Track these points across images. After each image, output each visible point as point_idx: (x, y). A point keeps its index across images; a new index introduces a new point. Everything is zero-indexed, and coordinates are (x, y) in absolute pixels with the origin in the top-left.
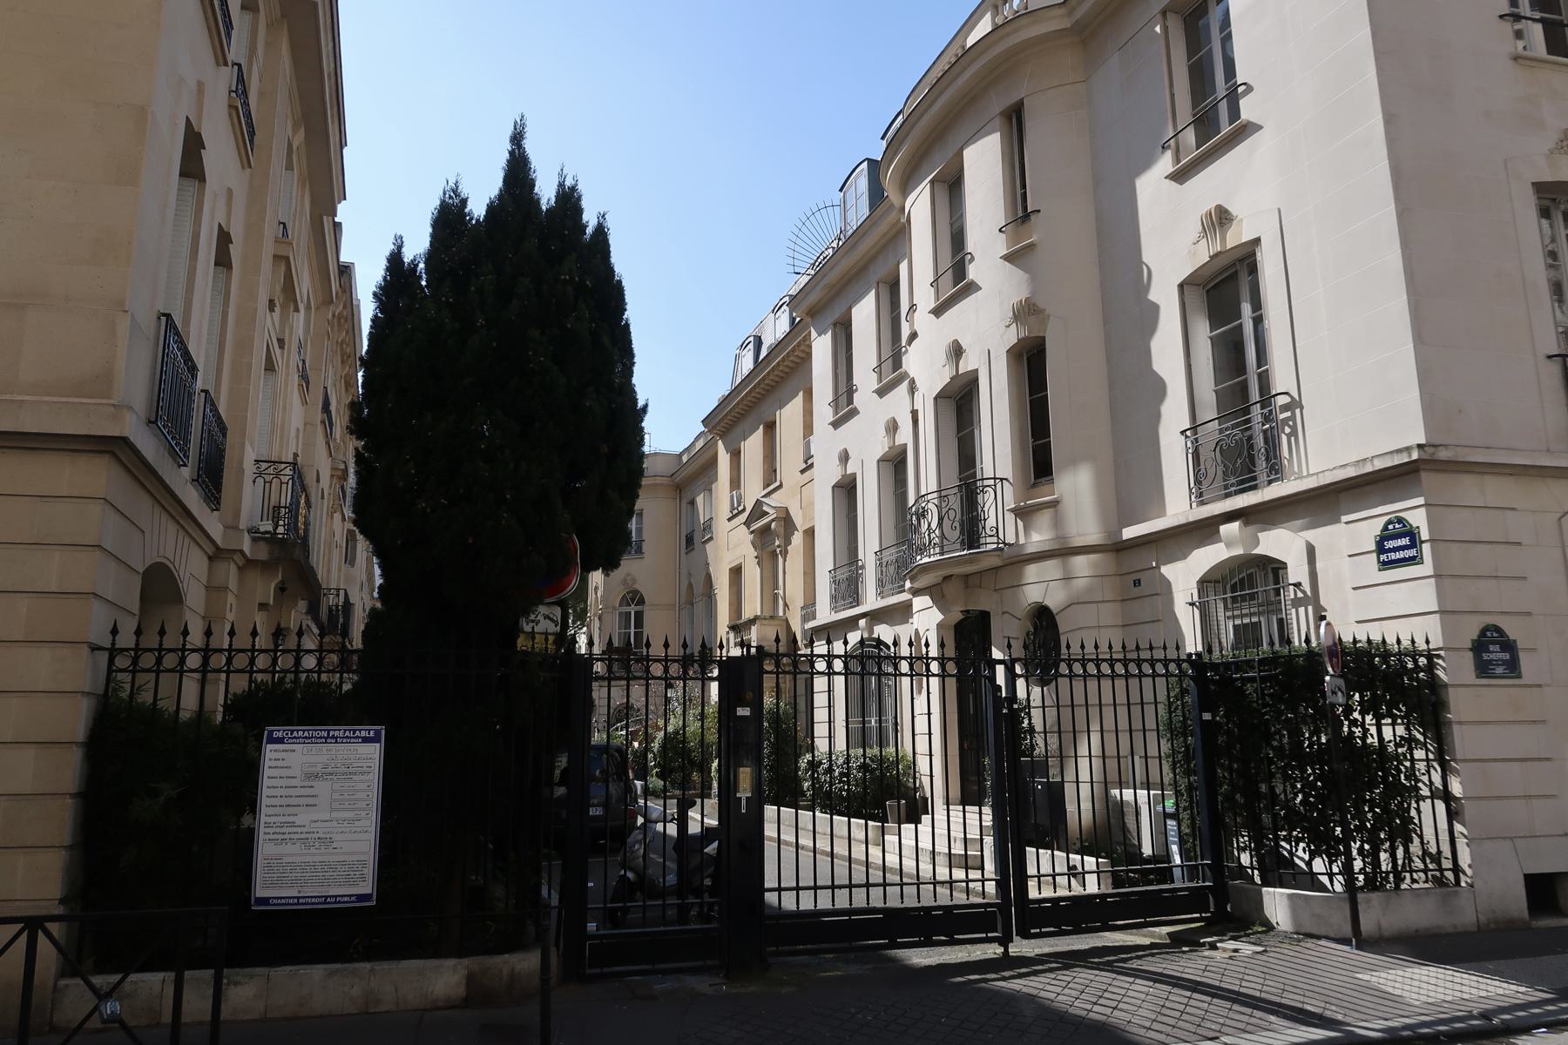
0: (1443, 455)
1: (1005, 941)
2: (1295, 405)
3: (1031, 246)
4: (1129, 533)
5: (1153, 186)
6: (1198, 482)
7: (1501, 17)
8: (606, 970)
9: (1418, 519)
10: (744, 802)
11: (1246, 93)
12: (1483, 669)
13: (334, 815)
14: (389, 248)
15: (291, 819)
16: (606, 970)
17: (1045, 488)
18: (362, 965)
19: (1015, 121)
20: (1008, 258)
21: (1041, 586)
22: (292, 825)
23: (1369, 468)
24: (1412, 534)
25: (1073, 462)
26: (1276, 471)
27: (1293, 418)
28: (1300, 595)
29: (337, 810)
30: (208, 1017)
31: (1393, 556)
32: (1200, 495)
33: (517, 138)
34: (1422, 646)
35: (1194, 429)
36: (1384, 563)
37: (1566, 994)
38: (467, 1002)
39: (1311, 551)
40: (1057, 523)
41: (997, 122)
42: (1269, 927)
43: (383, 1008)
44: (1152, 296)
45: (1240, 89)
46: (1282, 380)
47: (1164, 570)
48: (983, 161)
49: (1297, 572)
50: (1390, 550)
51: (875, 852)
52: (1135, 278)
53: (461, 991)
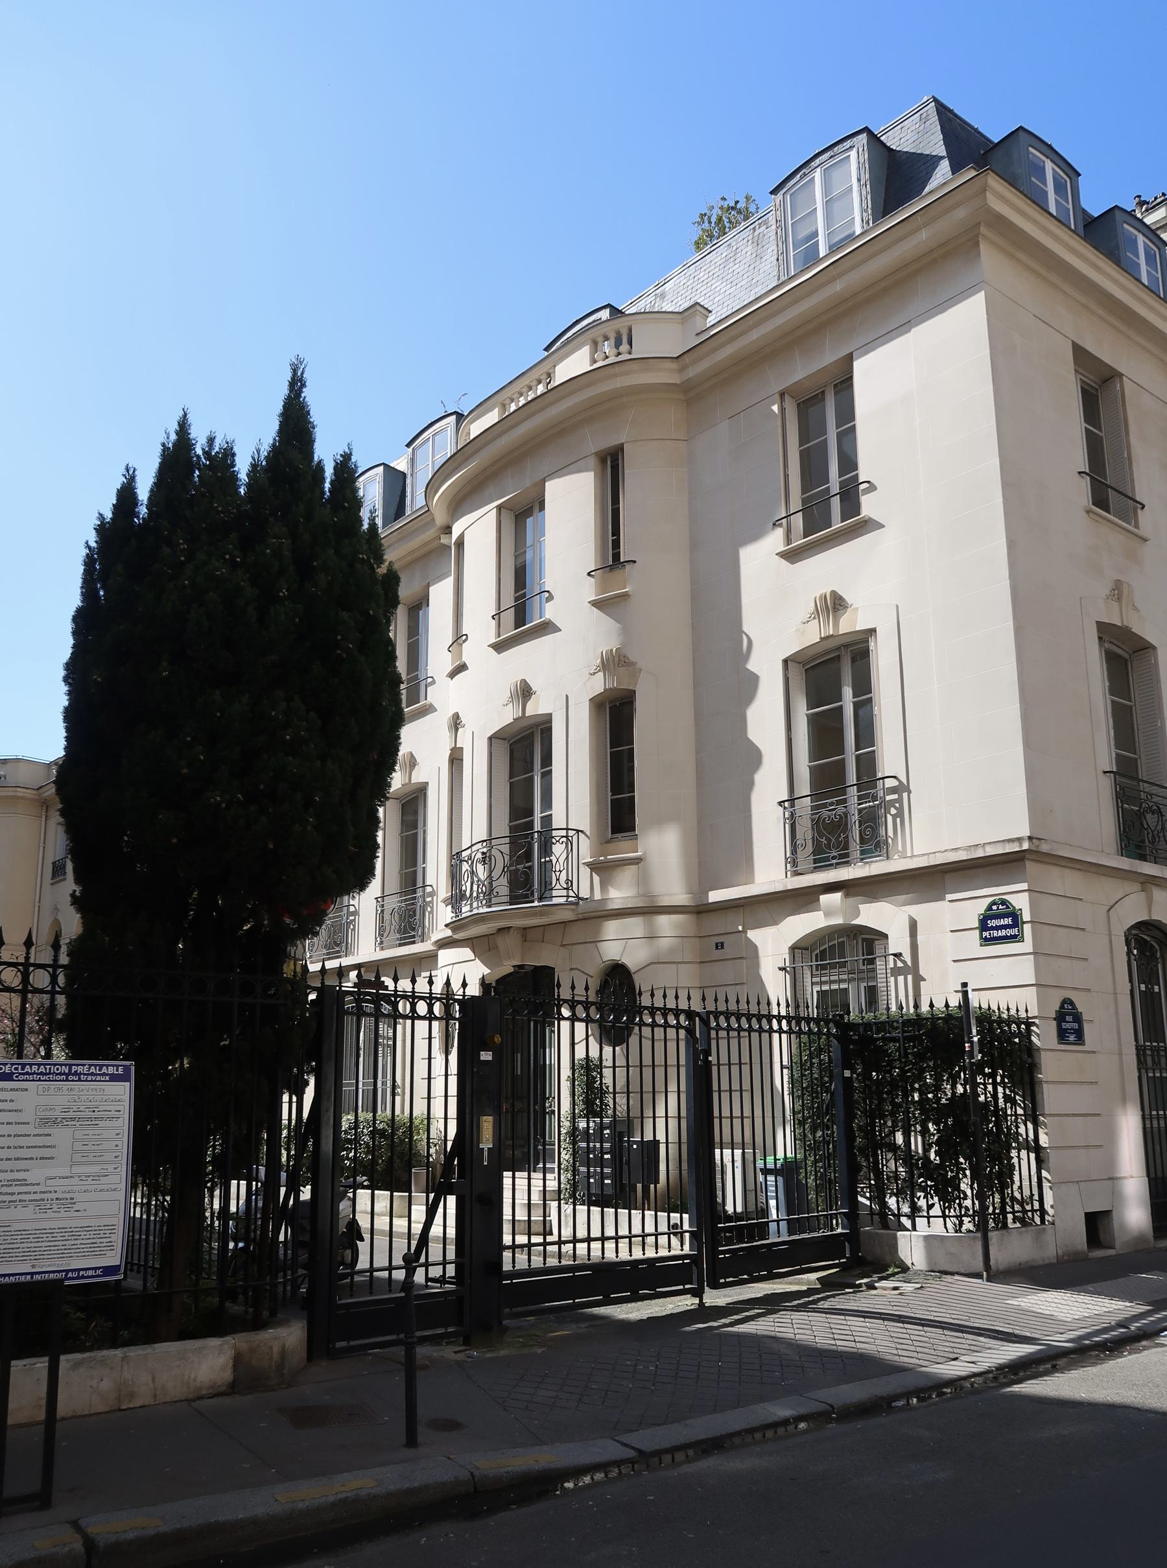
0: (1044, 848)
1: (698, 1293)
2: (902, 788)
3: (625, 596)
4: (715, 896)
5: (759, 556)
6: (794, 851)
7: (1080, 473)
8: (352, 1343)
9: (1021, 902)
10: (486, 1153)
11: (867, 491)
12: (1062, 1035)
13: (77, 1170)
14: (118, 481)
15: (21, 1175)
16: (352, 1343)
17: (624, 844)
18: (112, 1352)
19: (612, 465)
20: (595, 604)
21: (620, 943)
22: (24, 1183)
23: (980, 853)
24: (1015, 917)
25: (659, 821)
26: (874, 844)
27: (901, 798)
28: (900, 964)
29: (81, 1164)
30: (42, 1415)
31: (995, 934)
32: (793, 864)
33: (297, 384)
34: (1023, 1015)
35: (792, 801)
36: (986, 939)
37: (1158, 1305)
38: (233, 1388)
39: (913, 926)
40: (643, 880)
41: (592, 461)
42: (904, 1269)
43: (137, 1403)
44: (752, 666)
45: (862, 487)
46: (889, 763)
47: (751, 934)
48: (571, 501)
49: (898, 942)
50: (992, 928)
51: (400, 1224)
52: (736, 649)
53: (228, 1375)
